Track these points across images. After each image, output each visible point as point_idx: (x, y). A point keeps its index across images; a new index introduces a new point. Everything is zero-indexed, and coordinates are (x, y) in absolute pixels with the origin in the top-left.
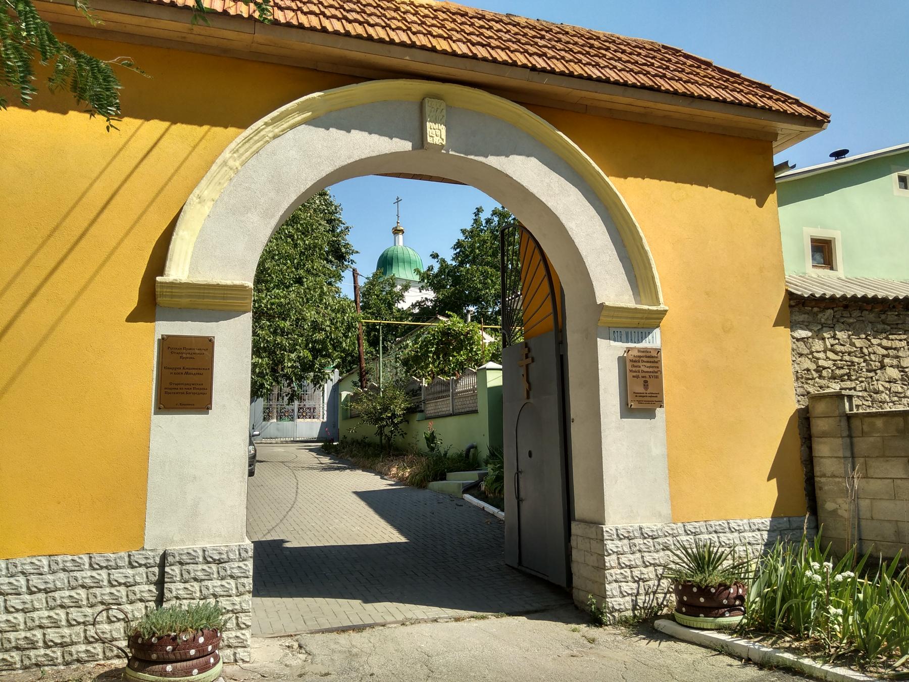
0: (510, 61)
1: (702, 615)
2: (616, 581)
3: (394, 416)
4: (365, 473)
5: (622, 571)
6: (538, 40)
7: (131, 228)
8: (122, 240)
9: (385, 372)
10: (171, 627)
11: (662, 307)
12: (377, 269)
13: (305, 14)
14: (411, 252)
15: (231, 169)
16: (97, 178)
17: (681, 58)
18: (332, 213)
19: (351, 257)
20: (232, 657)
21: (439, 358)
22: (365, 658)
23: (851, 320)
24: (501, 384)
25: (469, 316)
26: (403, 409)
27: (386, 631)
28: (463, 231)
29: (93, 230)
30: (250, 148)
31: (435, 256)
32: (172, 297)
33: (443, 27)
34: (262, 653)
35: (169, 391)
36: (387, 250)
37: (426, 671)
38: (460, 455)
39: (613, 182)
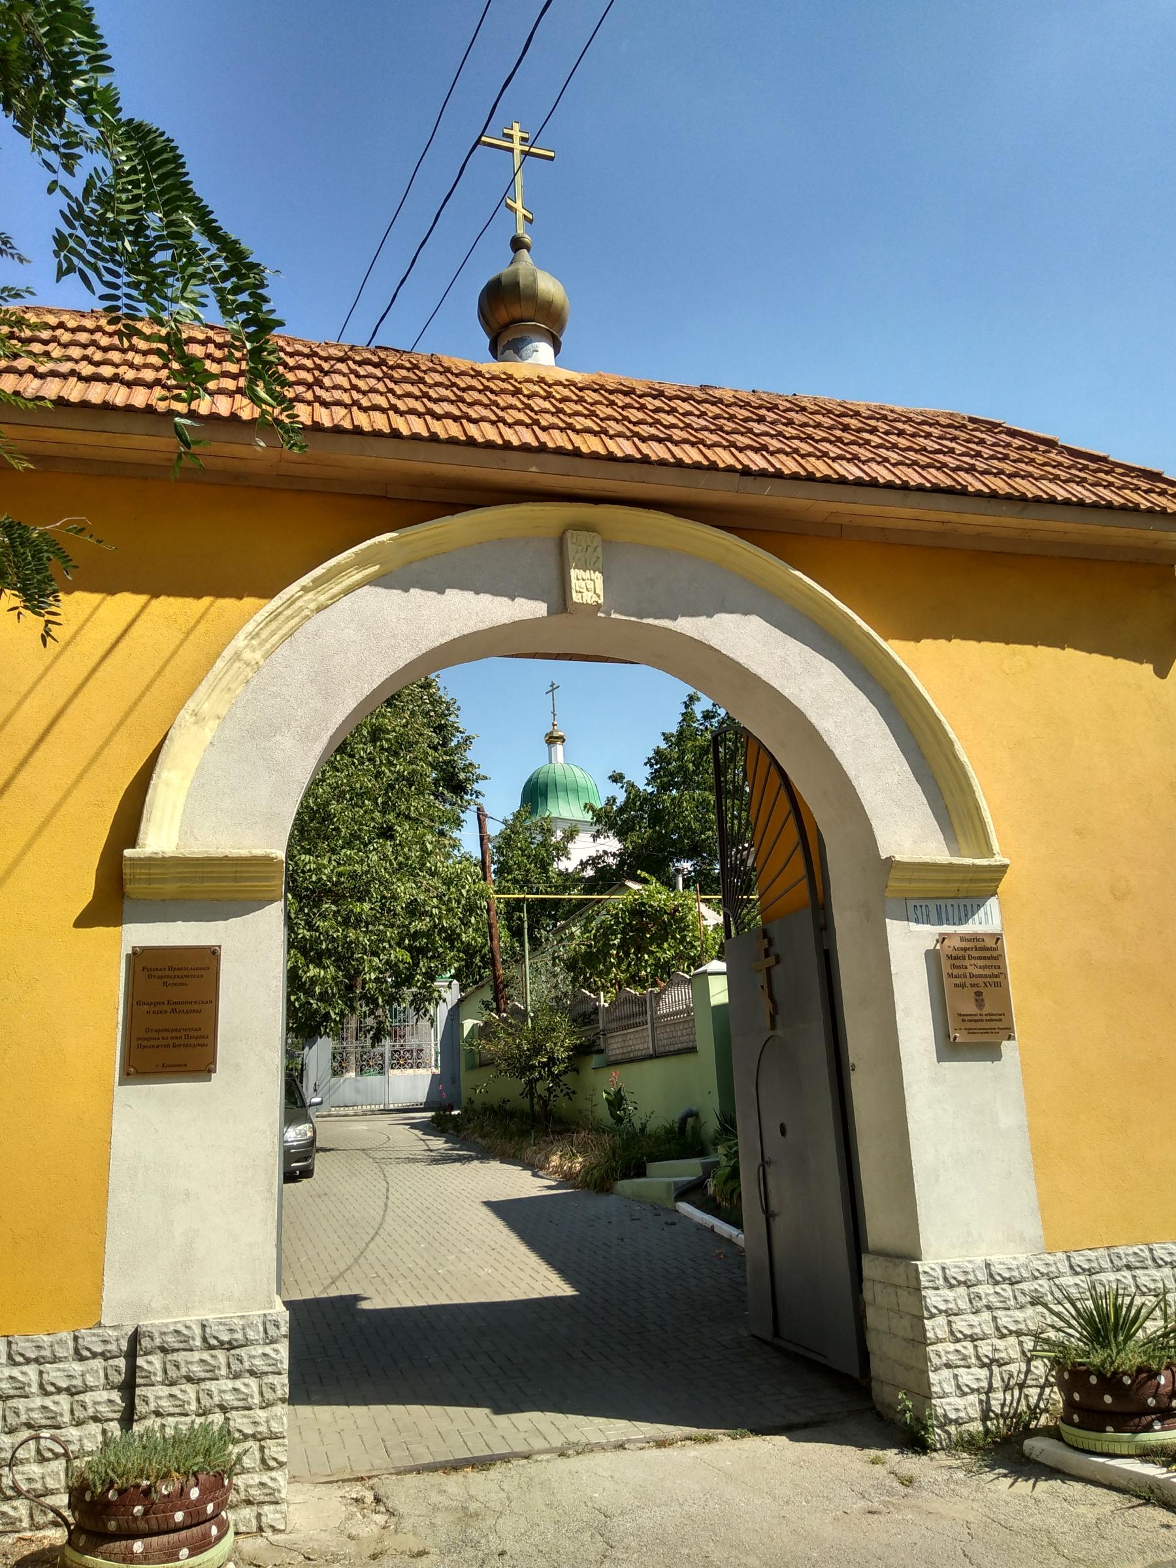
0: (705, 463)
1: (1110, 1428)
2: (948, 1366)
3: (552, 1061)
4: (505, 1166)
5: (958, 1346)
6: (755, 425)
7: (86, 770)
8: (69, 792)
9: (536, 983)
10: (142, 1470)
11: (997, 860)
12: (522, 806)
13: (365, 410)
14: (578, 772)
15: (248, 665)
16: (29, 692)
17: (1003, 437)
18: (443, 716)
19: (476, 787)
20: (254, 1523)
21: (627, 954)
22: (490, 1522)
24: (727, 1001)
25: (680, 879)
26: (568, 1049)
27: (531, 1468)
28: (667, 737)
29: (23, 778)
30: (279, 629)
31: (617, 778)
32: (150, 881)
33: (592, 414)
34: (307, 1513)
35: (145, 1043)
36: (538, 772)
37: (600, 1545)
38: (669, 1131)
39: (897, 650)
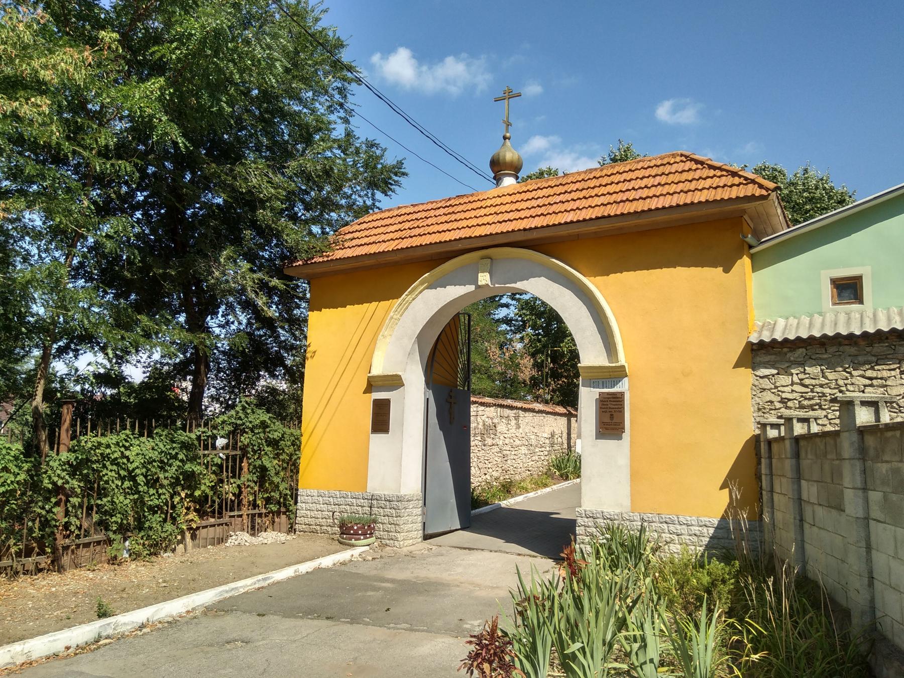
23: (825, 356)
